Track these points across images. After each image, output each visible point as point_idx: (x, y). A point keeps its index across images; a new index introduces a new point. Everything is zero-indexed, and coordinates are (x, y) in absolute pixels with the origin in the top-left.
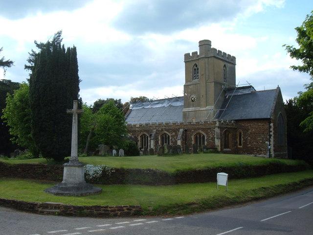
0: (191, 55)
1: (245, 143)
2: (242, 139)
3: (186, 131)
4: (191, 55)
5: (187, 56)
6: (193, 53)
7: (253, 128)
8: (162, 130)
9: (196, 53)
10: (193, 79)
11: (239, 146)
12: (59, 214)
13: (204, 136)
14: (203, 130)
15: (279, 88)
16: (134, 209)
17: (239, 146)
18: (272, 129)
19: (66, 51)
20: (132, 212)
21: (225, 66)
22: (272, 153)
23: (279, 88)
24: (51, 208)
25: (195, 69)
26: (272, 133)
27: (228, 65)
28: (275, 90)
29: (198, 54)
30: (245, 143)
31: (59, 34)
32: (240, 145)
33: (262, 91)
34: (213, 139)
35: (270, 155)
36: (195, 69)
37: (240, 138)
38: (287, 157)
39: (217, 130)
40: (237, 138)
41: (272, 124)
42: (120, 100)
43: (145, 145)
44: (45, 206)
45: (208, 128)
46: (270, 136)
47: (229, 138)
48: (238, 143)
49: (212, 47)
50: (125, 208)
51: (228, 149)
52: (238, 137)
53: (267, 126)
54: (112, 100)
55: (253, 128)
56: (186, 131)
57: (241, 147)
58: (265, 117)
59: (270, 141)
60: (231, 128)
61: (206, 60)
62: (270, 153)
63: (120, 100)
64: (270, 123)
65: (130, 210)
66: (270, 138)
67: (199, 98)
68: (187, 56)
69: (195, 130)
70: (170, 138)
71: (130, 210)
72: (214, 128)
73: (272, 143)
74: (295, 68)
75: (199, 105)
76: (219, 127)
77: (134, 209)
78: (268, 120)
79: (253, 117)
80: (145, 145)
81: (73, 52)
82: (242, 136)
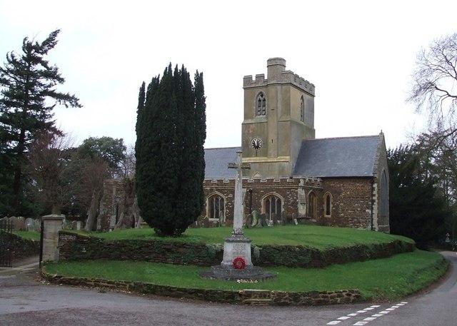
0: (254, 79)
1: (336, 212)
2: (331, 206)
3: (251, 191)
4: (254, 79)
5: (247, 80)
6: (258, 77)
7: (347, 190)
8: (211, 190)
9: (262, 76)
10: (256, 115)
11: (210, 219)
12: (271, 304)
13: (279, 201)
14: (278, 191)
15: (382, 133)
16: (353, 295)
17: (210, 219)
18: (375, 192)
19: (173, 73)
20: (352, 298)
21: (302, 97)
22: (376, 226)
23: (382, 133)
24: (256, 297)
25: (260, 100)
26: (375, 198)
27: (307, 97)
28: (376, 136)
29: (266, 78)
30: (336, 212)
31: (407, 101)
32: (328, 213)
33: (359, 137)
34: (295, 204)
35: (372, 228)
36: (260, 100)
37: (328, 205)
38: (389, 232)
39: (301, 192)
40: (323, 203)
41: (375, 185)
42: (121, 140)
43: (273, 211)
44: (249, 295)
45: (287, 188)
46: (373, 201)
47: (314, 204)
48: (325, 210)
49: (287, 69)
50: (344, 294)
51: (314, 220)
52: (325, 203)
53: (368, 187)
54: (109, 139)
55: (347, 190)
56: (251, 191)
57: (329, 216)
58: (366, 174)
59: (372, 209)
60: (317, 189)
61: (279, 87)
62: (372, 225)
63: (121, 140)
64: (373, 183)
65: (350, 295)
66: (373, 204)
67: (266, 143)
68: (247, 80)
69: (266, 191)
70: (225, 202)
71: (350, 295)
72: (297, 189)
73: (375, 211)
74: (170, 65)
75: (266, 154)
76: (303, 188)
77: (353, 295)
78: (370, 180)
79: (348, 174)
80: (273, 211)
81: (168, 72)
82: (331, 201)
